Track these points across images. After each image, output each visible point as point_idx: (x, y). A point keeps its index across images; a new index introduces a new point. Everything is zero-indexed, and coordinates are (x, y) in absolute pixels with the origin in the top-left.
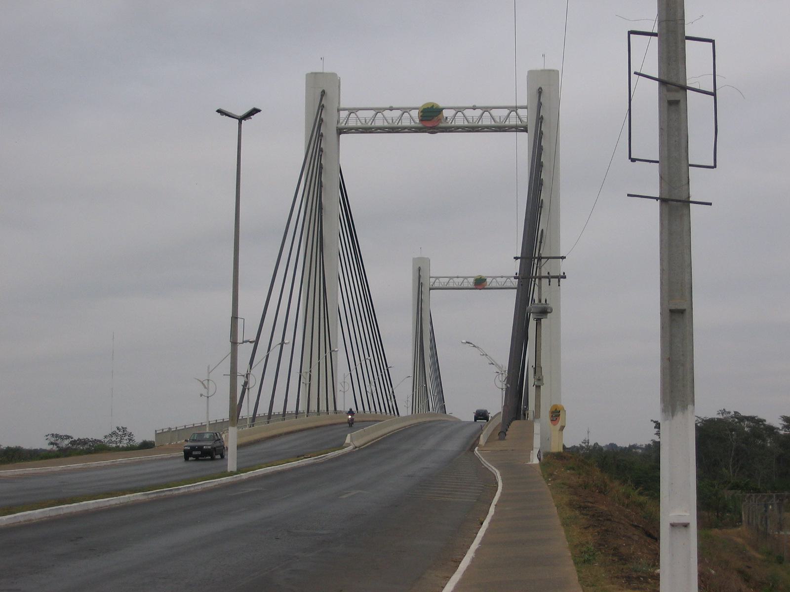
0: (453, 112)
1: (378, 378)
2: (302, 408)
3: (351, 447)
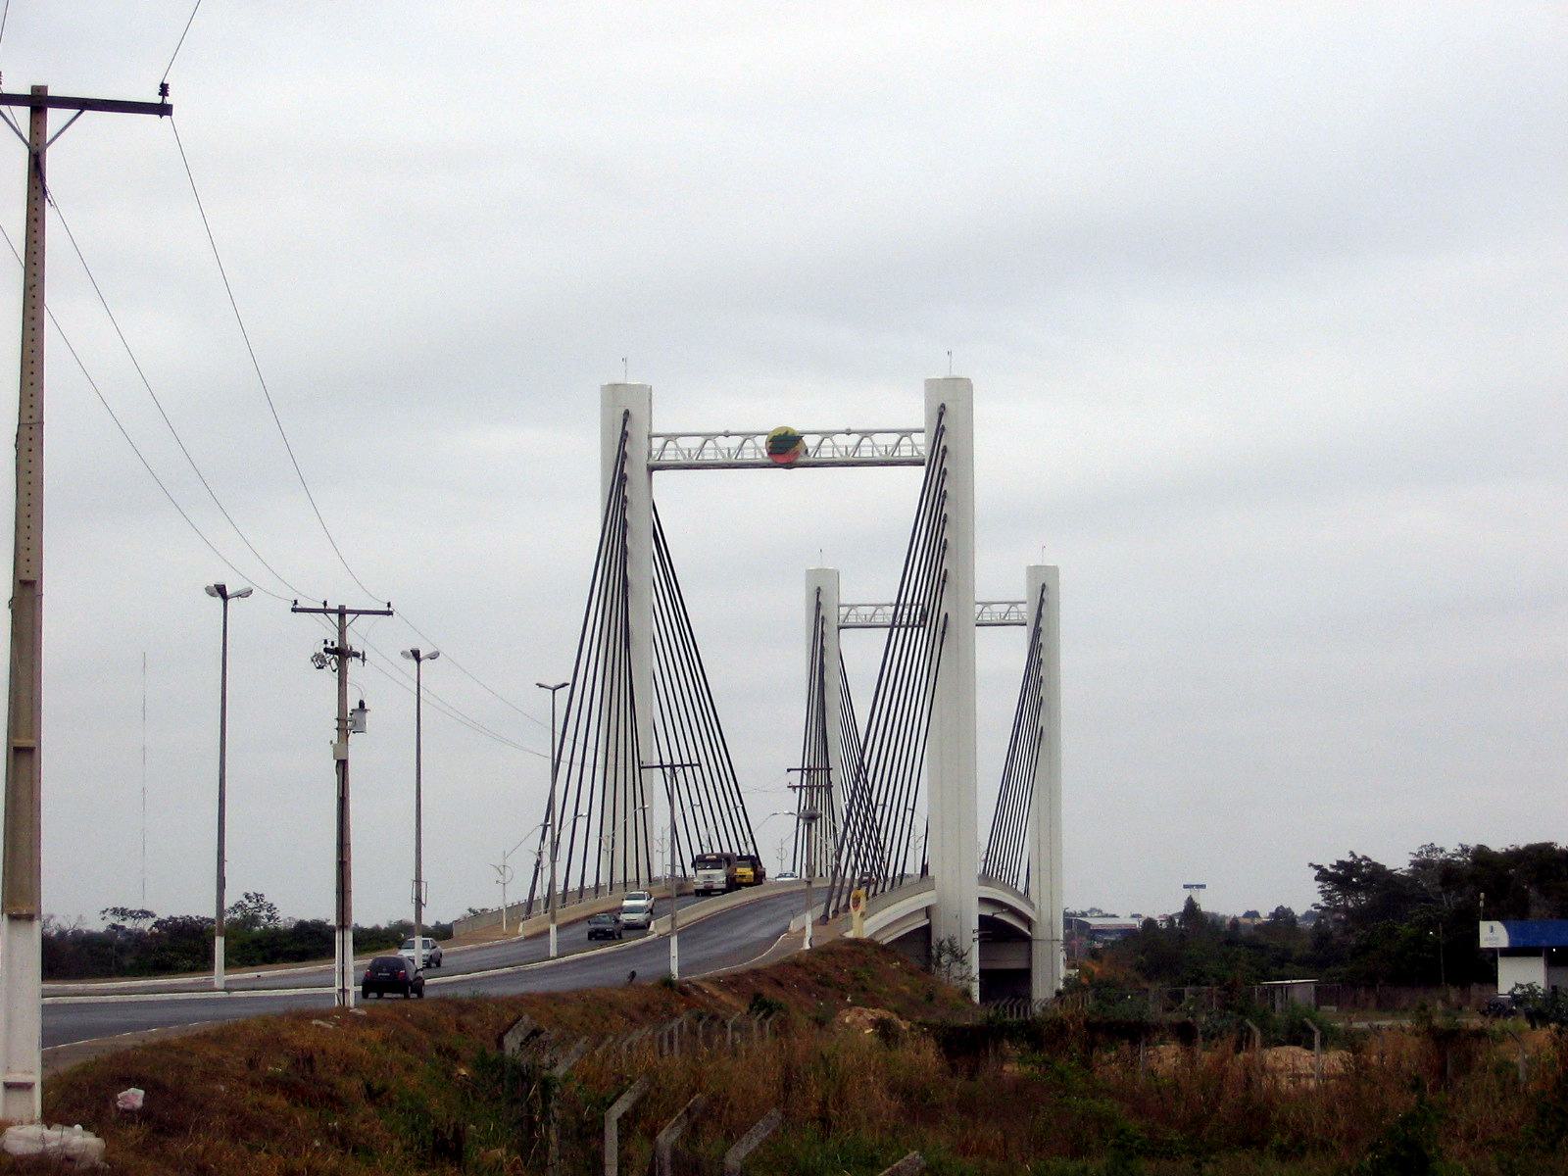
0: (817, 438)
1: (730, 814)
2: (604, 880)
3: (655, 935)
